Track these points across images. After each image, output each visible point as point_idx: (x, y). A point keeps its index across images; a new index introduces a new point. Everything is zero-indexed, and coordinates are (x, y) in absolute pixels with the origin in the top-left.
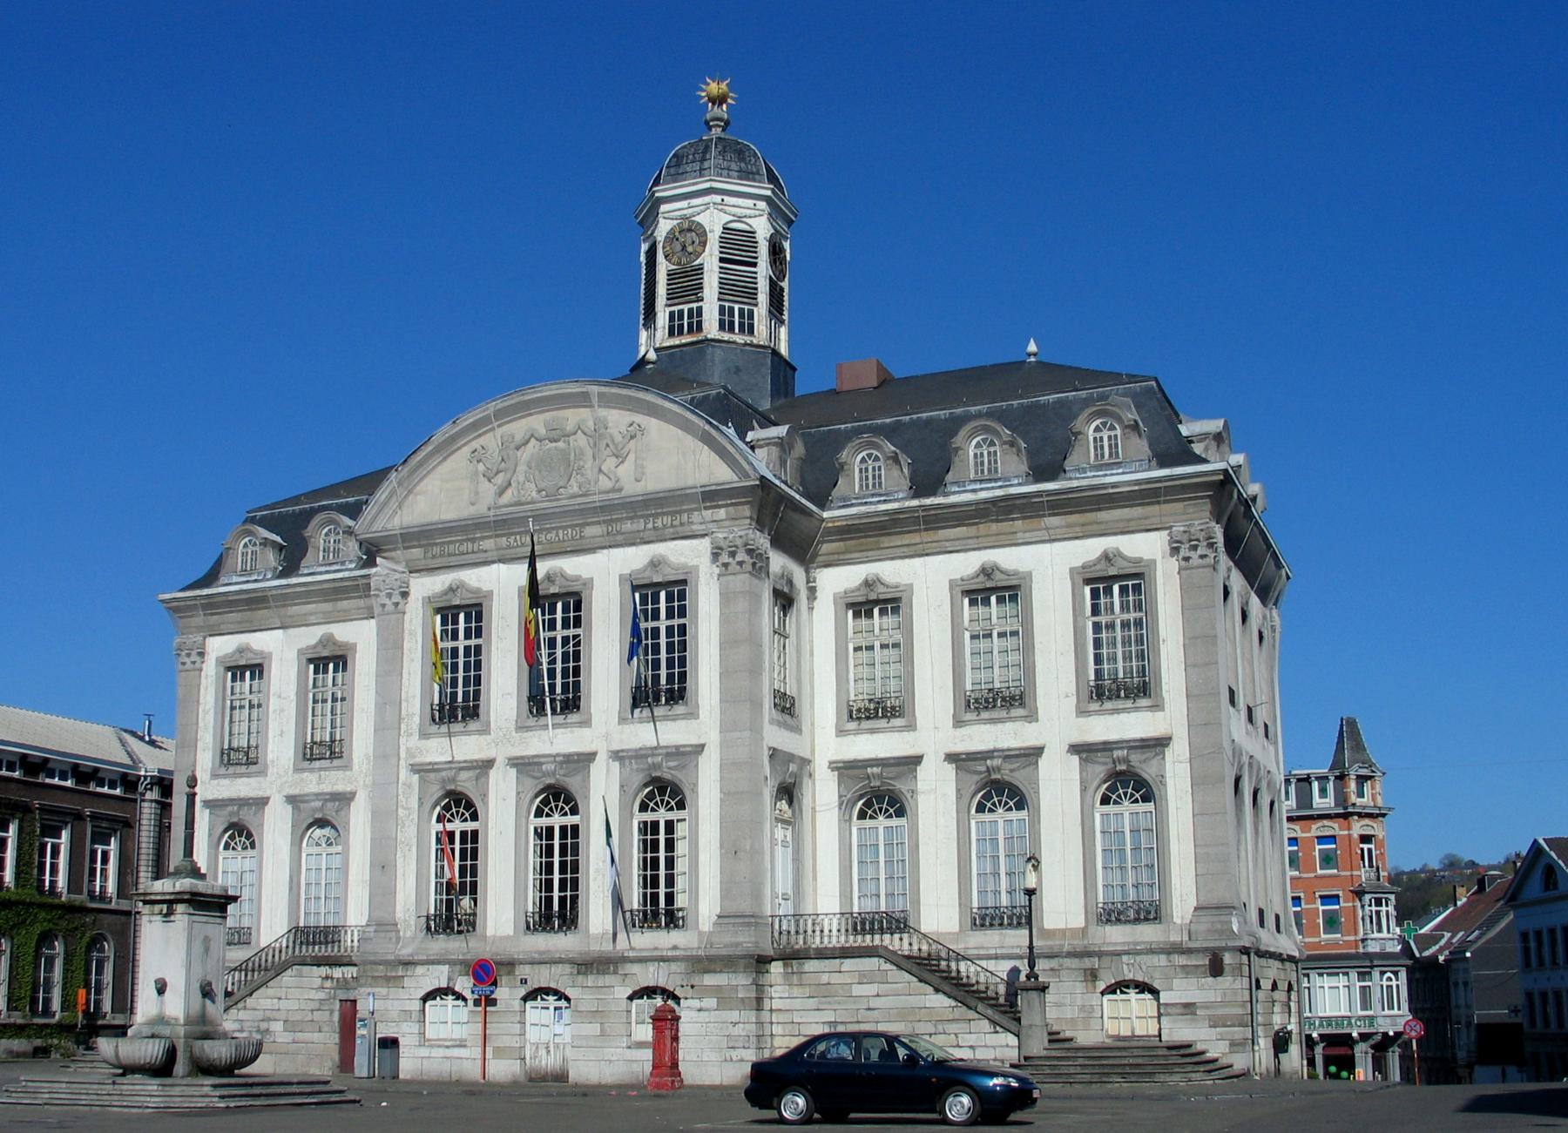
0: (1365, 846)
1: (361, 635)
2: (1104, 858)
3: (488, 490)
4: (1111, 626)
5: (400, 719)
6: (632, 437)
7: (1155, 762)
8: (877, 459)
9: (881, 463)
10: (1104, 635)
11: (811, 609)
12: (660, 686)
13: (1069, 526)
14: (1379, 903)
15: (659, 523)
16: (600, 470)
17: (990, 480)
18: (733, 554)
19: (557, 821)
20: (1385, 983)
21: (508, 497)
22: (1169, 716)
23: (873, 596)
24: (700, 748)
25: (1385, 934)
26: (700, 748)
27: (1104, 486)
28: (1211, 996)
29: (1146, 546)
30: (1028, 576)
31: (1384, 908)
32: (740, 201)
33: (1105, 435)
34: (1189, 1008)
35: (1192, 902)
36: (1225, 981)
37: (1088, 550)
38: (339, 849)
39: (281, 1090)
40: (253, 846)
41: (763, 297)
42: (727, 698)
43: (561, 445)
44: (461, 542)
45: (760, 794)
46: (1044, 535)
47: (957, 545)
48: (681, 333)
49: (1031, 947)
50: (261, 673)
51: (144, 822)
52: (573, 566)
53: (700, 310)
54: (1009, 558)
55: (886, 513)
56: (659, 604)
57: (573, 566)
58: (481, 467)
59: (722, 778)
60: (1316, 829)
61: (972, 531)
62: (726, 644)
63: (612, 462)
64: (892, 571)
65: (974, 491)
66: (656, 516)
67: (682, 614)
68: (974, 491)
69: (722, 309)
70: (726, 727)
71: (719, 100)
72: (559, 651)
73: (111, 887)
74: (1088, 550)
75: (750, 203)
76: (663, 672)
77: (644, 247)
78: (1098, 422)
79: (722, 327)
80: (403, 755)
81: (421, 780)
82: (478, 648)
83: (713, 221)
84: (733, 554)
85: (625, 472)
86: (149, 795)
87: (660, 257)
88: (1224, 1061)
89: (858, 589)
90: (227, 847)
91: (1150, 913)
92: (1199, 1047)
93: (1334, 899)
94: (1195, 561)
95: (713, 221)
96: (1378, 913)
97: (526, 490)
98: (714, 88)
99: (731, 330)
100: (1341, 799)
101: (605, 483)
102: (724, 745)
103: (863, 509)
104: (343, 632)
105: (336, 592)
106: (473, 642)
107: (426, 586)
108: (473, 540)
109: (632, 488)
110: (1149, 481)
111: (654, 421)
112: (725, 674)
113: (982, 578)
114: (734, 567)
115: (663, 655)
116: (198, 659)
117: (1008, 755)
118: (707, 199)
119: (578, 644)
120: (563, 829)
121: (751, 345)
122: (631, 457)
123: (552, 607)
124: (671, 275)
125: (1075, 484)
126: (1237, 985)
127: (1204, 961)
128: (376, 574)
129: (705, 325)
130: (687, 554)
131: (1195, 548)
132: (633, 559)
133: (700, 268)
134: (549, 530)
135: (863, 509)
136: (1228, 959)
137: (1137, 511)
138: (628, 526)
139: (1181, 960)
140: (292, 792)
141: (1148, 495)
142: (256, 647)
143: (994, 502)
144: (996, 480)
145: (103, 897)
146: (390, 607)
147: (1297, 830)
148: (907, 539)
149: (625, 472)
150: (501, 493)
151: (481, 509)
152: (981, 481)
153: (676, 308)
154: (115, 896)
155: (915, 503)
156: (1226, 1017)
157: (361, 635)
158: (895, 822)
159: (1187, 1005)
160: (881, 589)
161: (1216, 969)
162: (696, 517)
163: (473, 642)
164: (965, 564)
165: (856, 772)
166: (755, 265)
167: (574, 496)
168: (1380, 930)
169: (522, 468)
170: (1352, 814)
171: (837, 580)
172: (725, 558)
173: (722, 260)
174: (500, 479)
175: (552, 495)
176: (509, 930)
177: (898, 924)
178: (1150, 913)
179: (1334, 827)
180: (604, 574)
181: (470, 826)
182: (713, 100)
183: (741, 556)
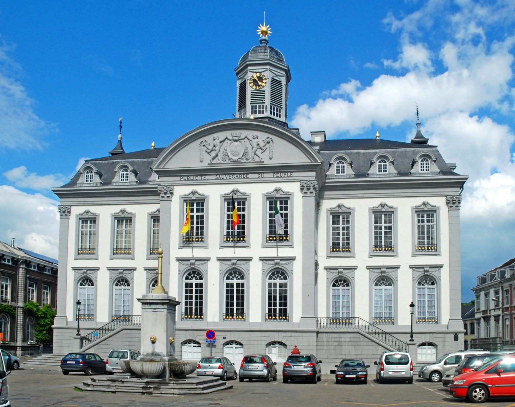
2: (333, 298)
6: (269, 143)
12: (278, 235)
16: (255, 154)
22: (443, 258)
30: (412, 208)
39: (187, 392)
40: (93, 285)
44: (197, 176)
49: (412, 331)
50: (95, 221)
51: (20, 275)
56: (278, 204)
71: (264, 33)
73: (9, 297)
77: (239, 83)
82: (202, 217)
86: (22, 266)
98: (264, 28)
106: (200, 214)
107: (182, 191)
109: (267, 162)
113: (380, 208)
114: (309, 194)
117: (432, 267)
120: (238, 285)
123: (236, 204)
124: (252, 92)
142: (92, 211)
145: (6, 301)
150: (214, 158)
153: (254, 105)
154: (10, 301)
158: (346, 288)
163: (200, 214)
174: (213, 154)
176: (217, 320)
177: (349, 320)
178: (435, 320)
180: (257, 193)
182: (262, 32)
183: (312, 190)
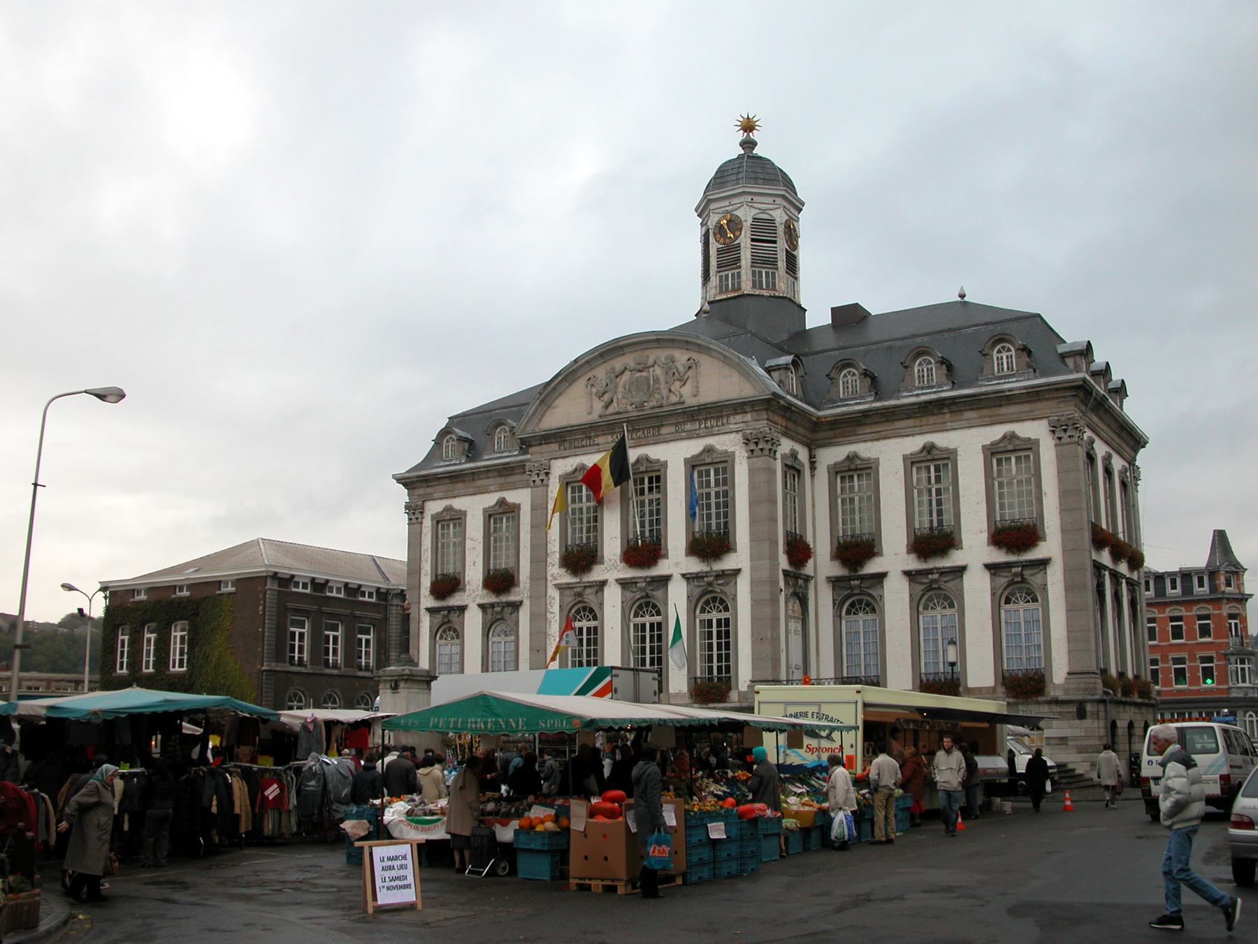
0: (1233, 622)
1: (521, 497)
3: (598, 406)
4: (1010, 483)
5: (547, 555)
7: (1040, 576)
8: (854, 374)
9: (856, 378)
10: (1006, 489)
11: (812, 476)
13: (980, 417)
14: (1242, 662)
15: (708, 424)
17: (929, 387)
18: (757, 444)
19: (647, 620)
20: (1247, 719)
21: (611, 410)
23: (853, 467)
24: (738, 571)
25: (1247, 684)
26: (738, 571)
27: (1003, 391)
28: (1077, 733)
29: (1035, 429)
31: (1246, 666)
32: (764, 200)
33: (1004, 355)
34: (1063, 740)
35: (1065, 669)
36: (1087, 723)
37: (995, 433)
38: (512, 638)
41: (782, 264)
42: (754, 538)
43: (644, 374)
45: (778, 601)
46: (964, 423)
47: (908, 431)
48: (727, 290)
52: (655, 452)
53: (739, 274)
54: (942, 440)
55: (860, 411)
57: (655, 452)
58: (594, 390)
59: (752, 591)
60: (1169, 612)
61: (917, 422)
62: (753, 504)
63: (678, 384)
64: (866, 450)
65: (917, 395)
66: (706, 419)
67: (725, 483)
68: (917, 395)
69: (754, 272)
70: (754, 557)
72: (647, 509)
74: (995, 433)
75: (770, 200)
76: (714, 521)
78: (999, 347)
79: (754, 286)
80: (549, 578)
81: (561, 594)
83: (746, 215)
84: (757, 444)
85: (687, 391)
87: (712, 239)
88: (1087, 776)
89: (843, 462)
90: (441, 638)
91: (951, 685)
92: (1070, 766)
93: (1210, 659)
94: (1066, 440)
95: (746, 215)
96: (1243, 669)
97: (622, 404)
99: (761, 288)
100: (1214, 588)
101: (674, 399)
102: (752, 569)
103: (844, 409)
104: (512, 497)
105: (505, 471)
107: (562, 466)
108: (590, 438)
109: (691, 401)
110: (1032, 387)
111: (703, 356)
112: (753, 523)
114: (758, 452)
115: (713, 510)
116: (419, 516)
118: (742, 199)
119: (658, 504)
121: (775, 297)
122: (689, 381)
125: (984, 389)
126: (1096, 725)
127: (1073, 709)
128: (529, 460)
129: (743, 286)
130: (728, 442)
131: (1065, 431)
132: (693, 447)
133: (739, 246)
134: (638, 430)
135: (844, 409)
136: (1089, 708)
137: (1026, 407)
138: (688, 427)
139: (1057, 709)
140: (481, 602)
141: (1034, 395)
143: (930, 402)
144: (932, 387)
146: (538, 482)
147: (1156, 613)
148: (875, 428)
149: (687, 391)
150: (607, 407)
151: (594, 417)
152: (922, 388)
155: (878, 404)
156: (1087, 747)
157: (521, 497)
159: (1061, 738)
160: (858, 462)
161: (1081, 714)
162: (732, 420)
164: (913, 444)
165: (843, 584)
166: (775, 242)
167: (653, 408)
168: (1244, 681)
169: (620, 389)
170: (1221, 599)
171: (832, 455)
172: (752, 447)
173: (753, 240)
174: (606, 397)
175: (640, 407)
179: (1210, 609)
180: (673, 455)
181: (593, 624)
